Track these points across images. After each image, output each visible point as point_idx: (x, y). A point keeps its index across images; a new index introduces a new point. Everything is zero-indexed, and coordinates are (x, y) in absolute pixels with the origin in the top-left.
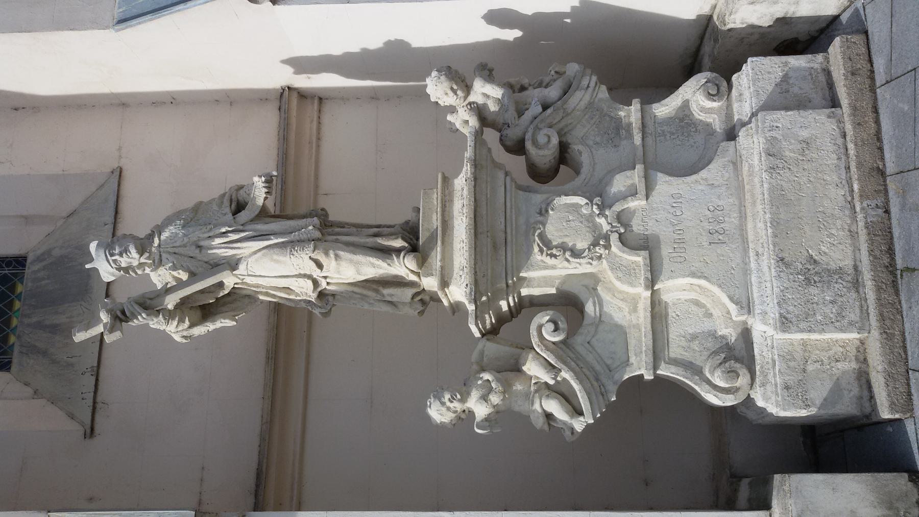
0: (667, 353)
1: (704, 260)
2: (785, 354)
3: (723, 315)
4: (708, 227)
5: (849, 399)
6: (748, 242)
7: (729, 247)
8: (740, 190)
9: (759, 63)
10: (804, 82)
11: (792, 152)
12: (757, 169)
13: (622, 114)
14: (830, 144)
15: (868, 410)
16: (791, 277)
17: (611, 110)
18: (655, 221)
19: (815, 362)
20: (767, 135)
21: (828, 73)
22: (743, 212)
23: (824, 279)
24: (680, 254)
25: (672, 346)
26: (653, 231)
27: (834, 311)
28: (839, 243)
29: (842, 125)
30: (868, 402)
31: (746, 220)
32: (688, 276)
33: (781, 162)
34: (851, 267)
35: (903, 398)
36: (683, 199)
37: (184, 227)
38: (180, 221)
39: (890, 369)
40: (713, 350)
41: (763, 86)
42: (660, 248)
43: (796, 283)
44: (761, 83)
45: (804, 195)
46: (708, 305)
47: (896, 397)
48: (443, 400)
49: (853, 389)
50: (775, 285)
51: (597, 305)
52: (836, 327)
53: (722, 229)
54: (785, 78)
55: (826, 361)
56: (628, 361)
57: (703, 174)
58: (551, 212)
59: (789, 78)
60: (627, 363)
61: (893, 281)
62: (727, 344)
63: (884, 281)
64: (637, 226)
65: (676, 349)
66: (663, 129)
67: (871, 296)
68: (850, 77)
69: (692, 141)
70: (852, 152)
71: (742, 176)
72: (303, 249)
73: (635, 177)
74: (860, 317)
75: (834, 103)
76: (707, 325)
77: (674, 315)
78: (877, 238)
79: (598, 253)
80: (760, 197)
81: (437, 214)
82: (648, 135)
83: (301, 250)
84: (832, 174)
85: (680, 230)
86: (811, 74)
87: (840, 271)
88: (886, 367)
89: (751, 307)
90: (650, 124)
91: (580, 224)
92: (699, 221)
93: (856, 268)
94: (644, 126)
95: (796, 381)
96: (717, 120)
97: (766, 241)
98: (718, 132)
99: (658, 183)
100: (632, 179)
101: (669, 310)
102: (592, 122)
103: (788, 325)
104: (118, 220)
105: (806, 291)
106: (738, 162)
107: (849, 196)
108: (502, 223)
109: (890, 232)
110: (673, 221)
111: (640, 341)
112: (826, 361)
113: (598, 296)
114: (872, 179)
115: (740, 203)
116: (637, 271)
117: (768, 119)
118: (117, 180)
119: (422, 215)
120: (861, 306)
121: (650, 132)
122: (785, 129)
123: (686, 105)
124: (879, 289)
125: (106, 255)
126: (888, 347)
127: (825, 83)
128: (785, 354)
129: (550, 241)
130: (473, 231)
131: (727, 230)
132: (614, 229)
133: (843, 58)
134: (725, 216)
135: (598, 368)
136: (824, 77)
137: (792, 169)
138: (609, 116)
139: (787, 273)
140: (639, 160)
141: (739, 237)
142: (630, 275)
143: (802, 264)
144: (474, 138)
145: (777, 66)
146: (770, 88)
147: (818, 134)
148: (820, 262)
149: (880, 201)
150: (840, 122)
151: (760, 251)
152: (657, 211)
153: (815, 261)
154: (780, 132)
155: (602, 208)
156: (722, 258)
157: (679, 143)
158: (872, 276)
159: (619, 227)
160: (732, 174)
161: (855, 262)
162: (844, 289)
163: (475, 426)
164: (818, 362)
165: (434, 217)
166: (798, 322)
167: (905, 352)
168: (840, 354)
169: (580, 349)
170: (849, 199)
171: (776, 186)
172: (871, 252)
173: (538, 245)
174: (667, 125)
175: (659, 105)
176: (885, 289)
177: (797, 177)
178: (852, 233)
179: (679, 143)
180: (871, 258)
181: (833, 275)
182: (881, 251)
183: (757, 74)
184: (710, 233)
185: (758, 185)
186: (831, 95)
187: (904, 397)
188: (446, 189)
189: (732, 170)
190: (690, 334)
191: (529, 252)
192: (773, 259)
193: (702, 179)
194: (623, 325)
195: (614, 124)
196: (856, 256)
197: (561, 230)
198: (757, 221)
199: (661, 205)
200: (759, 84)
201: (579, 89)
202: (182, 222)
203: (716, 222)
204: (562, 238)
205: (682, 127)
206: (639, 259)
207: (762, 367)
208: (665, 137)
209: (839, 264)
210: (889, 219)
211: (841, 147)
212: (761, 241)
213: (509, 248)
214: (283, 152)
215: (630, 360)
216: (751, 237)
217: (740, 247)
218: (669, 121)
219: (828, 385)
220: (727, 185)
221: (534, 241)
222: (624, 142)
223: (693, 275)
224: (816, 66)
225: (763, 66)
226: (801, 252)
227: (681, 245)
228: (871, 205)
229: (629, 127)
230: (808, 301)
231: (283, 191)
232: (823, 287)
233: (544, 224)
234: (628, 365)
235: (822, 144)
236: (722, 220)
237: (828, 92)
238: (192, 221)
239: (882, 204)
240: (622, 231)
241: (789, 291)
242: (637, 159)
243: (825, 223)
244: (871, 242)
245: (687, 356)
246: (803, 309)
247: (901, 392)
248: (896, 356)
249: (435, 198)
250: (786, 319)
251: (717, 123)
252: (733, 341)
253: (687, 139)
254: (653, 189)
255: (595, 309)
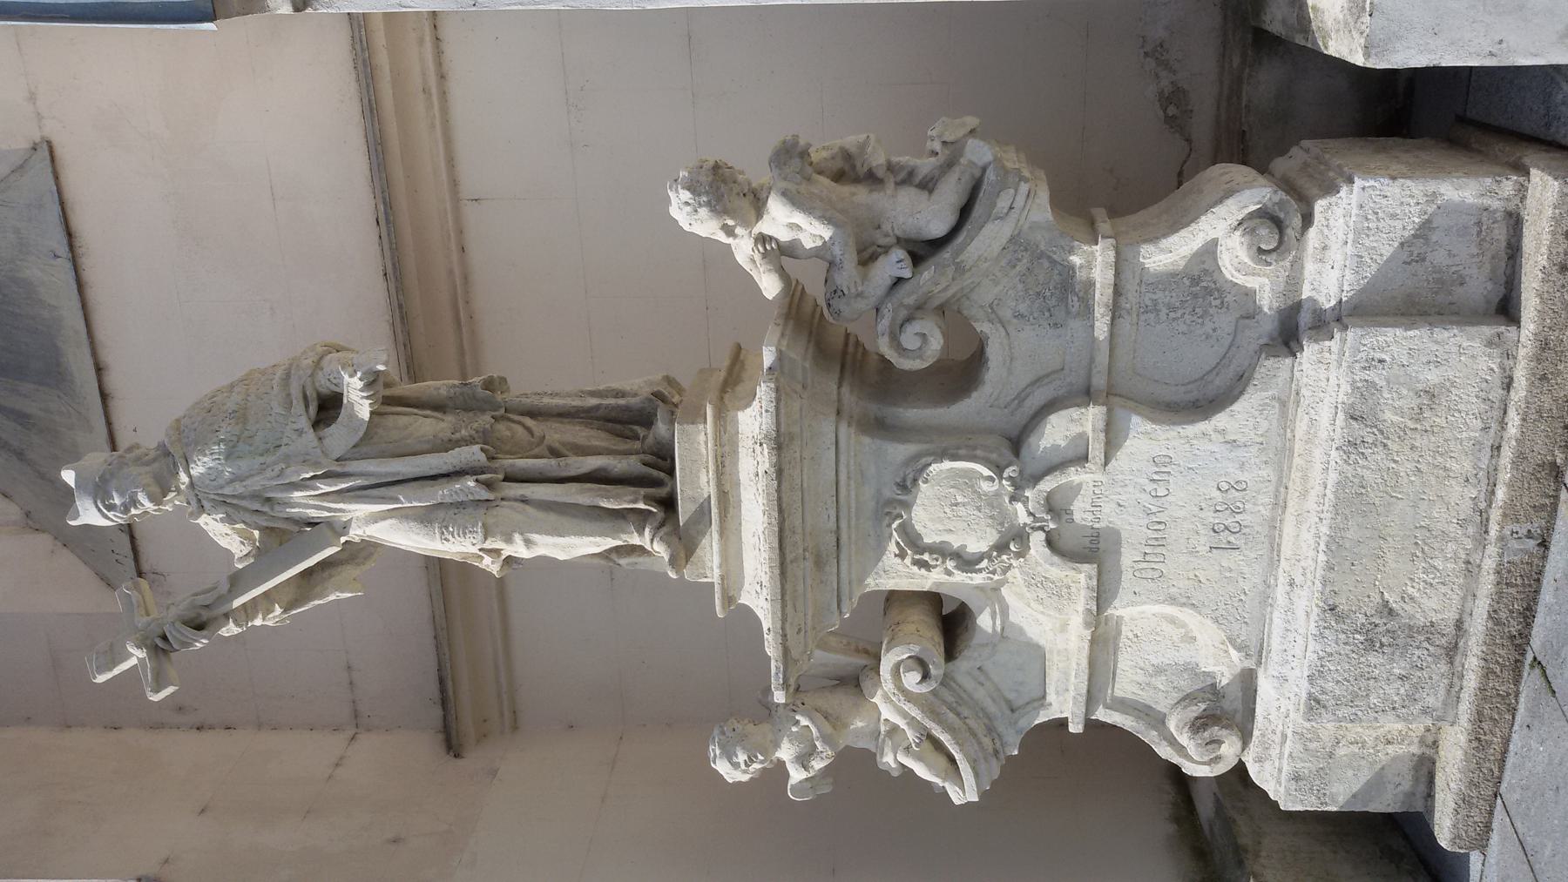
0: (1110, 691)
1: (1196, 576)
2: (1305, 731)
3: (1213, 645)
4: (1212, 520)
5: (1392, 796)
6: (1279, 551)
7: (1244, 556)
8: (1281, 454)
9: (1378, 193)
10: (1460, 239)
11: (1397, 414)
12: (1323, 435)
13: (1076, 260)
14: (1475, 400)
15: (1419, 806)
16: (1342, 636)
17: (1054, 249)
18: (1115, 506)
19: (1351, 743)
20: (1357, 378)
21: (1515, 222)
22: (1282, 497)
23: (1399, 641)
24: (1153, 566)
25: (1120, 680)
26: (1110, 522)
27: (1402, 691)
28: (1442, 583)
29: (1511, 362)
30: (1423, 800)
31: (1283, 512)
32: (1163, 602)
33: (1373, 433)
34: (1451, 623)
35: (1475, 830)
36: (1173, 466)
37: (229, 456)
38: (219, 445)
39: (1469, 791)
40: (1189, 691)
41: (1375, 245)
42: (1119, 553)
43: (1348, 647)
44: (1371, 238)
45: (1400, 496)
46: (1191, 626)
47: (1465, 828)
48: (735, 759)
49: (1403, 783)
50: (1310, 648)
51: (998, 616)
52: (1398, 716)
53: (1237, 525)
54: (1426, 228)
55: (1370, 743)
56: (1044, 697)
57: (1221, 420)
58: (923, 486)
59: (1430, 229)
60: (1041, 700)
61: (1517, 661)
62: (1213, 685)
63: (1500, 660)
64: (1081, 512)
65: (1127, 683)
66: (1154, 297)
67: (1471, 681)
68: (1555, 276)
69: (1209, 327)
70: (1513, 430)
71: (1293, 431)
72: (465, 534)
73: (1089, 419)
74: (1445, 704)
75: (1506, 309)
76: (1184, 655)
77: (1131, 635)
78: (1510, 590)
79: (1006, 563)
80: (1319, 489)
81: (708, 472)
82: (1123, 313)
83: (461, 535)
84: (1463, 458)
85: (1160, 523)
86: (1479, 223)
87: (1430, 629)
88: (1463, 788)
89: (1264, 657)
90: (1131, 287)
91: (975, 512)
92: (1197, 509)
93: (1459, 625)
94: (1118, 291)
95: (1314, 769)
96: (1267, 289)
97: (1312, 569)
98: (1265, 314)
99: (1130, 436)
100: (1082, 425)
101: (1123, 627)
102: (1013, 273)
103: (1319, 711)
104: (80, 251)
105: (1362, 659)
106: (1291, 402)
107: (1483, 500)
108: (831, 518)
109: (1538, 580)
110: (1150, 506)
111: (1066, 674)
112: (1370, 743)
113: (1002, 601)
114: (1535, 484)
115: (1280, 478)
116: (1073, 589)
117: (1365, 345)
118: (50, 170)
119: (680, 473)
120: (1451, 686)
121: (1128, 306)
122: (1395, 366)
123: (1210, 250)
124: (1488, 673)
125: (99, 510)
126: (1475, 761)
127: (1504, 244)
128: (1305, 731)
129: (919, 536)
130: (777, 572)
131: (1245, 527)
132: (1038, 524)
133: (1553, 233)
134: (1247, 501)
135: (992, 708)
136: (1505, 231)
137: (1390, 447)
138: (1049, 257)
139: (1337, 631)
140: (1099, 372)
141: (1266, 540)
142: (1060, 596)
143: (1366, 615)
144: (773, 395)
145: (1412, 202)
146: (1387, 251)
147: (1459, 378)
148: (1399, 612)
149: (1537, 525)
150: (1508, 355)
151: (1299, 579)
152: (1121, 486)
153: (1391, 612)
154: (1384, 372)
155: (1019, 485)
156: (1228, 574)
157: (1183, 328)
158: (1483, 652)
159: (1046, 521)
160: (1275, 423)
161: (1461, 614)
162: (1429, 659)
163: (789, 791)
164: (1357, 743)
165: (703, 479)
166: (1336, 707)
167: (1502, 769)
168: (1396, 733)
169: (968, 684)
170: (1483, 505)
171: (1351, 479)
172: (1493, 615)
173: (898, 543)
174: (1164, 290)
175: (1153, 248)
176: (1499, 673)
177: (1395, 462)
178: (1470, 566)
179: (1183, 328)
180: (1490, 625)
181: (1415, 635)
182: (1511, 612)
183: (1367, 219)
184: (1215, 531)
185: (1318, 467)
186: (1508, 272)
187: (1478, 829)
188: (722, 433)
189: (1276, 416)
190: (1153, 665)
191: (880, 550)
192: (1317, 605)
193: (1216, 431)
194: (1041, 644)
195: (1056, 278)
196: (1465, 606)
197: (940, 520)
198: (1304, 527)
199: (1132, 477)
200: (1367, 242)
201: (992, 218)
202: (222, 446)
203: (1228, 512)
204: (940, 535)
205: (1195, 296)
206: (1081, 578)
207: (1263, 735)
208: (1158, 315)
209: (1432, 617)
210: (1544, 557)
211: (1496, 406)
212: (1303, 563)
213: (843, 556)
214: (375, 140)
215: (1047, 698)
216: (1286, 550)
217: (1265, 557)
218: (1170, 279)
219: (1365, 775)
220: (1262, 444)
221: (891, 535)
222: (1075, 325)
223: (1172, 600)
224: (1496, 204)
225: (1384, 202)
226: (1369, 597)
227: (1159, 550)
228: (1517, 533)
229: (1086, 292)
230: (1361, 676)
231: (391, 225)
232: (1393, 654)
233: (908, 506)
234: (1042, 705)
235: (1461, 398)
236: (1239, 508)
237: (1504, 265)
238: (240, 443)
239: (1539, 531)
240: (1052, 526)
241: (1333, 658)
242: (1094, 371)
243: (1426, 548)
244: (1499, 596)
245: (1145, 697)
246: (1351, 688)
247: (1475, 823)
248: (1484, 774)
249: (702, 443)
250: (1318, 702)
251: (1268, 299)
252: (1223, 683)
253: (1200, 321)
254: (1119, 446)
255: (994, 623)
